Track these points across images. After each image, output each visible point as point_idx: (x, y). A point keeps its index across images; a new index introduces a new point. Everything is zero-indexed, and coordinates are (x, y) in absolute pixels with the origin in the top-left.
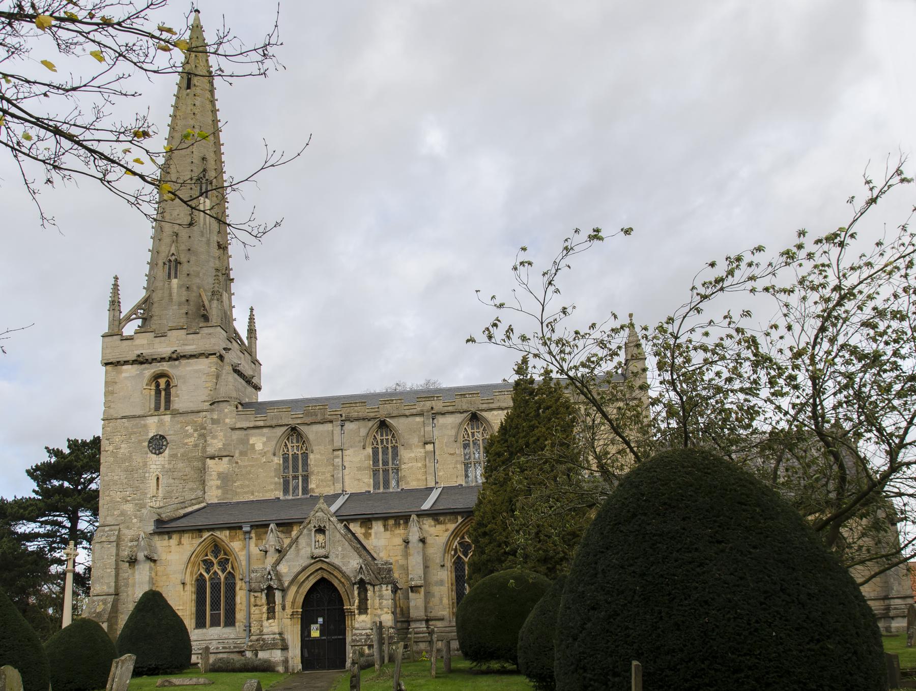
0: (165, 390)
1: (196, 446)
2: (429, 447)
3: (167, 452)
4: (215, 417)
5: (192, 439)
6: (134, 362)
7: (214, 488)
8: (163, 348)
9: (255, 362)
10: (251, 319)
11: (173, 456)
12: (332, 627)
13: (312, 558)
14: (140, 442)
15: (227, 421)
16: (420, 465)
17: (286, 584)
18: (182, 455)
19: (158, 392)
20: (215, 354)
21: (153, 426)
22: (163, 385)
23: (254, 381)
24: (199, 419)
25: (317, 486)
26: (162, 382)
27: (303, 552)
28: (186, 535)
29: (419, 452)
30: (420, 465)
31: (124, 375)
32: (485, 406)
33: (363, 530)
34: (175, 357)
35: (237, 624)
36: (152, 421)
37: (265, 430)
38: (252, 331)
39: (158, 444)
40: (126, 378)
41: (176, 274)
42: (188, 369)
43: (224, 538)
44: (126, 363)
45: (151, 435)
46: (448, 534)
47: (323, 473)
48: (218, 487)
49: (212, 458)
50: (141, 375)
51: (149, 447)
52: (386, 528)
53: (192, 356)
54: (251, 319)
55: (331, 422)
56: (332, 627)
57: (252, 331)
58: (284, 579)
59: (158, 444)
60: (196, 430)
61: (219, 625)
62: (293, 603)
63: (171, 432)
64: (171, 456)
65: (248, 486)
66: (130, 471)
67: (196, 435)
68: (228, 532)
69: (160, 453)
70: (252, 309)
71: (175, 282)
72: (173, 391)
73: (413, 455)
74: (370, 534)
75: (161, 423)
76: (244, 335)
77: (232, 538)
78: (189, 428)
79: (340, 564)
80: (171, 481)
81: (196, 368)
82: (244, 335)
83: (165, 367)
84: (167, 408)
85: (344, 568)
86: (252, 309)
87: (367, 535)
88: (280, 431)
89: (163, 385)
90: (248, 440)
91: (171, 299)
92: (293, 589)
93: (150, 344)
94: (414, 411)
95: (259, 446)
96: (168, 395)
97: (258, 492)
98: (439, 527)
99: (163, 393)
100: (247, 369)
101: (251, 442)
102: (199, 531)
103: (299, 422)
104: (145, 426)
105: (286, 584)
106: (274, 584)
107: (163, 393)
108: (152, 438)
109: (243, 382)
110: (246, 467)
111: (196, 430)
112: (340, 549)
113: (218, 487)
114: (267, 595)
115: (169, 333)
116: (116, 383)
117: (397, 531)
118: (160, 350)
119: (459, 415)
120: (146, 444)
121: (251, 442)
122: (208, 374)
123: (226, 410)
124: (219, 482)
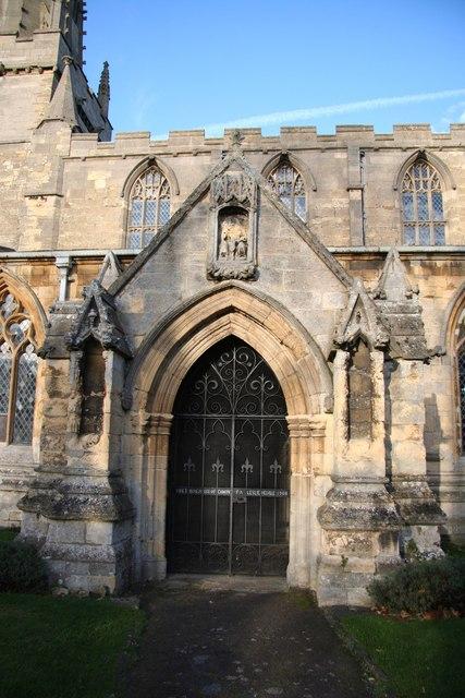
1: (15, 187)
2: (356, 195)
4: (43, 141)
10: (105, 75)
12: (247, 466)
13: (211, 276)
15: (59, 147)
16: (340, 220)
17: (139, 341)
20: (51, 68)
24: (23, 151)
29: (340, 202)
30: (340, 220)
32: (438, 143)
35: (36, 440)
37: (112, 162)
38: (104, 87)
42: (13, 87)
49: (32, 197)
53: (19, 71)
54: (105, 75)
56: (247, 466)
58: (133, 326)
60: (16, 166)
62: (152, 394)
65: (80, 239)
67: (16, 172)
70: (106, 65)
73: (330, 206)
76: (94, 87)
78: (8, 163)
79: (285, 301)
81: (26, 86)
82: (94, 87)
85: (296, 311)
86: (106, 65)
88: (132, 163)
90: (86, 174)
92: (156, 358)
95: (100, 184)
101: (90, 177)
105: (139, 341)
106: (103, 332)
110: (79, 212)
111: (16, 166)
119: (398, 153)
121: (90, 177)
122: (40, 95)
123: (58, 133)
124: (39, 231)
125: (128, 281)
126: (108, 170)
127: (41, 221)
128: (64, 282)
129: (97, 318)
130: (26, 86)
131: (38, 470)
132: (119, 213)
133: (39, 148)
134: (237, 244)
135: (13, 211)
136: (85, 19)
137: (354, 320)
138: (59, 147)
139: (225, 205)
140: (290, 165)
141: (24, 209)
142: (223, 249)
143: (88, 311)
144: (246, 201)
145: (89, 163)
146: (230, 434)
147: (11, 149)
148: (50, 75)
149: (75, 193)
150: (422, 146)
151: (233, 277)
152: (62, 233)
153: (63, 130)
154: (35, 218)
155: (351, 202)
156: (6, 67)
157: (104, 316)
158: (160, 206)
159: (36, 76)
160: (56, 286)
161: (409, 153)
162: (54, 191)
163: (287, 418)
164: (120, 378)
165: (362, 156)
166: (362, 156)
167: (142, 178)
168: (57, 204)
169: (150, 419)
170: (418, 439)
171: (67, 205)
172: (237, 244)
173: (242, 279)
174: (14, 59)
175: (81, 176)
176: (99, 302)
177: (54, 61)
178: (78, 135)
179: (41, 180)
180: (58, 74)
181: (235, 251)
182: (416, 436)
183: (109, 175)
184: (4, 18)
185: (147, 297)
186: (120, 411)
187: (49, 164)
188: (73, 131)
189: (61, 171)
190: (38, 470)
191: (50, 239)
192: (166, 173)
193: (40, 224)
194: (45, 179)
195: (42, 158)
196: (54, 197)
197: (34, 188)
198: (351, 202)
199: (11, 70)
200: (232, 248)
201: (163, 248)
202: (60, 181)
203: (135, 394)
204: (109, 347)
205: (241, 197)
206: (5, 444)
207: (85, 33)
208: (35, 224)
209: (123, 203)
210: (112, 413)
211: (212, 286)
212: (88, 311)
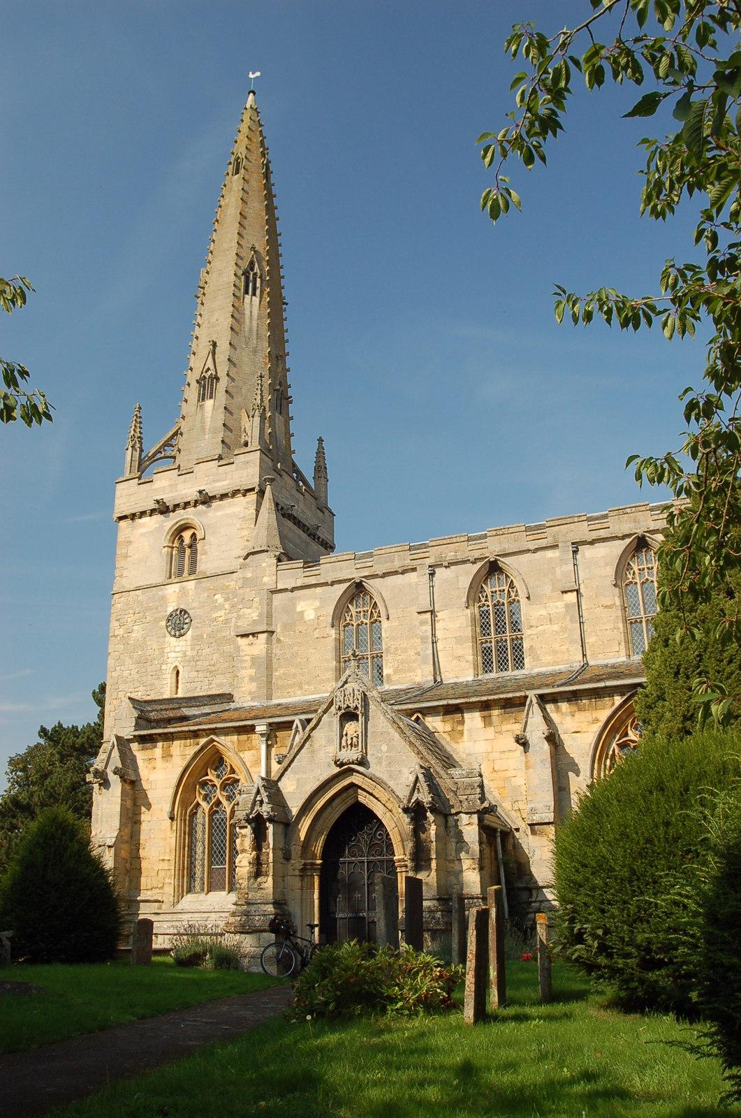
0: (190, 547)
1: (227, 621)
3: (190, 633)
4: (249, 575)
5: (222, 613)
6: (153, 512)
7: (246, 680)
8: (187, 490)
9: (323, 508)
10: (320, 454)
11: (197, 638)
14: (157, 620)
15: (266, 579)
16: (556, 627)
17: (295, 811)
18: (209, 636)
19: (182, 551)
20: (253, 489)
21: (173, 597)
22: (187, 540)
23: (322, 534)
24: (232, 582)
25: (396, 671)
26: (187, 535)
27: (321, 754)
28: (177, 743)
31: (142, 531)
33: (448, 728)
34: (206, 499)
36: (172, 590)
37: (319, 590)
38: (320, 469)
39: (179, 622)
40: (143, 535)
41: (211, 393)
42: (219, 514)
43: (229, 744)
44: (143, 514)
45: (170, 610)
46: (597, 728)
47: (405, 650)
48: (252, 679)
49: (242, 636)
50: (161, 527)
51: (167, 627)
52: (487, 721)
53: (224, 496)
54: (320, 454)
55: (414, 570)
57: (320, 469)
59: (179, 622)
61: (224, 889)
63: (195, 605)
64: (193, 638)
65: (294, 676)
66: (143, 662)
67: (227, 606)
68: (235, 738)
69: (181, 635)
70: (321, 440)
71: (209, 403)
72: (199, 546)
73: (544, 612)
74: (461, 733)
75: (183, 593)
76: (309, 474)
77: (241, 747)
80: (194, 674)
81: (228, 511)
83: (189, 515)
84: (193, 571)
85: (391, 783)
86: (321, 440)
87: (457, 734)
89: (187, 540)
90: (294, 605)
91: (203, 429)
93: (173, 486)
94: (543, 543)
95: (310, 615)
96: (194, 553)
97: (308, 683)
98: (580, 716)
99: (188, 551)
100: (310, 518)
101: (299, 609)
102: (195, 734)
103: (367, 574)
104: (163, 598)
107: (188, 551)
108: (171, 615)
109: (304, 536)
111: (227, 599)
112: (384, 748)
113: (252, 679)
114: (255, 831)
115: (196, 468)
116: (130, 542)
117: (506, 727)
118: (184, 492)
120: (163, 623)
121: (299, 609)
123: (264, 565)
124: (252, 672)
125: (286, 770)
126: (316, 598)
127: (254, 660)
128: (264, 747)
129: (262, 802)
130: (228, 511)
131: (235, 904)
132: (330, 643)
133: (246, 582)
134: (352, 739)
135: (227, 648)
136: (291, 402)
137: (416, 792)
138: (266, 579)
139: (343, 711)
140: (500, 570)
141: (238, 648)
142: (344, 743)
143: (256, 797)
144: (356, 708)
145: (297, 593)
146: (364, 871)
147: (221, 580)
148: (252, 497)
149: (286, 626)
150: (640, 532)
151: (350, 763)
152: (276, 670)
153: (268, 561)
154: (248, 658)
155: (567, 606)
156: (210, 495)
157: (266, 800)
158: (371, 630)
159: (239, 499)
160: (259, 750)
161: (628, 541)
162: (264, 628)
163: (395, 858)
164: (281, 838)
165: (575, 552)
166: (575, 552)
167: (351, 602)
168: (269, 642)
169: (305, 865)
170: (474, 869)
171: (279, 641)
172: (352, 739)
173: (356, 764)
174: (218, 484)
175: (289, 609)
176: (262, 790)
177: (254, 481)
178: (286, 565)
179: (251, 616)
180: (261, 493)
181: (351, 744)
182: (474, 866)
183: (317, 604)
184: (207, 437)
185: (298, 780)
186: (282, 860)
187: (257, 599)
188: (279, 560)
189: (270, 604)
190: (235, 904)
191: (265, 679)
192: (377, 599)
193: (253, 663)
194: (255, 616)
195: (249, 593)
196: (265, 635)
197: (245, 627)
198: (567, 606)
199: (214, 497)
200: (349, 742)
201: (307, 745)
202: (269, 616)
203: (293, 848)
204: (271, 820)
205: (352, 705)
206: (224, 893)
207: (292, 418)
208: (248, 664)
209: (333, 632)
210: (274, 862)
211: (338, 770)
212: (256, 797)
